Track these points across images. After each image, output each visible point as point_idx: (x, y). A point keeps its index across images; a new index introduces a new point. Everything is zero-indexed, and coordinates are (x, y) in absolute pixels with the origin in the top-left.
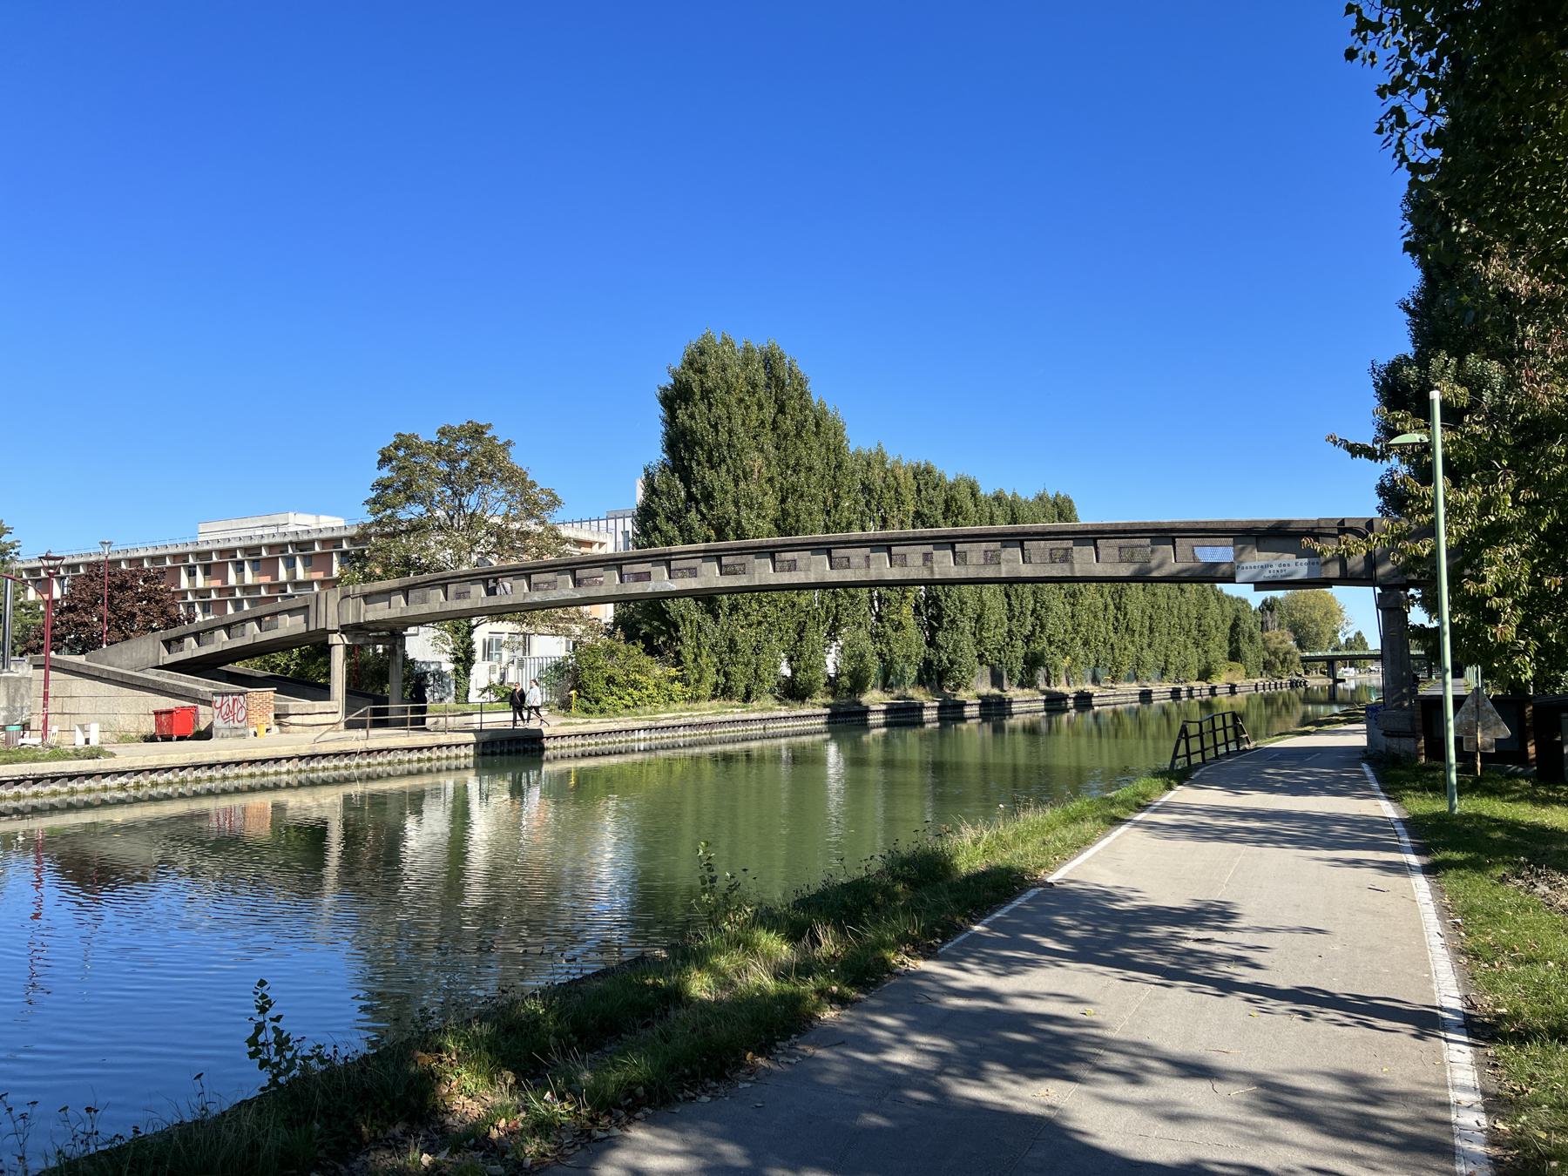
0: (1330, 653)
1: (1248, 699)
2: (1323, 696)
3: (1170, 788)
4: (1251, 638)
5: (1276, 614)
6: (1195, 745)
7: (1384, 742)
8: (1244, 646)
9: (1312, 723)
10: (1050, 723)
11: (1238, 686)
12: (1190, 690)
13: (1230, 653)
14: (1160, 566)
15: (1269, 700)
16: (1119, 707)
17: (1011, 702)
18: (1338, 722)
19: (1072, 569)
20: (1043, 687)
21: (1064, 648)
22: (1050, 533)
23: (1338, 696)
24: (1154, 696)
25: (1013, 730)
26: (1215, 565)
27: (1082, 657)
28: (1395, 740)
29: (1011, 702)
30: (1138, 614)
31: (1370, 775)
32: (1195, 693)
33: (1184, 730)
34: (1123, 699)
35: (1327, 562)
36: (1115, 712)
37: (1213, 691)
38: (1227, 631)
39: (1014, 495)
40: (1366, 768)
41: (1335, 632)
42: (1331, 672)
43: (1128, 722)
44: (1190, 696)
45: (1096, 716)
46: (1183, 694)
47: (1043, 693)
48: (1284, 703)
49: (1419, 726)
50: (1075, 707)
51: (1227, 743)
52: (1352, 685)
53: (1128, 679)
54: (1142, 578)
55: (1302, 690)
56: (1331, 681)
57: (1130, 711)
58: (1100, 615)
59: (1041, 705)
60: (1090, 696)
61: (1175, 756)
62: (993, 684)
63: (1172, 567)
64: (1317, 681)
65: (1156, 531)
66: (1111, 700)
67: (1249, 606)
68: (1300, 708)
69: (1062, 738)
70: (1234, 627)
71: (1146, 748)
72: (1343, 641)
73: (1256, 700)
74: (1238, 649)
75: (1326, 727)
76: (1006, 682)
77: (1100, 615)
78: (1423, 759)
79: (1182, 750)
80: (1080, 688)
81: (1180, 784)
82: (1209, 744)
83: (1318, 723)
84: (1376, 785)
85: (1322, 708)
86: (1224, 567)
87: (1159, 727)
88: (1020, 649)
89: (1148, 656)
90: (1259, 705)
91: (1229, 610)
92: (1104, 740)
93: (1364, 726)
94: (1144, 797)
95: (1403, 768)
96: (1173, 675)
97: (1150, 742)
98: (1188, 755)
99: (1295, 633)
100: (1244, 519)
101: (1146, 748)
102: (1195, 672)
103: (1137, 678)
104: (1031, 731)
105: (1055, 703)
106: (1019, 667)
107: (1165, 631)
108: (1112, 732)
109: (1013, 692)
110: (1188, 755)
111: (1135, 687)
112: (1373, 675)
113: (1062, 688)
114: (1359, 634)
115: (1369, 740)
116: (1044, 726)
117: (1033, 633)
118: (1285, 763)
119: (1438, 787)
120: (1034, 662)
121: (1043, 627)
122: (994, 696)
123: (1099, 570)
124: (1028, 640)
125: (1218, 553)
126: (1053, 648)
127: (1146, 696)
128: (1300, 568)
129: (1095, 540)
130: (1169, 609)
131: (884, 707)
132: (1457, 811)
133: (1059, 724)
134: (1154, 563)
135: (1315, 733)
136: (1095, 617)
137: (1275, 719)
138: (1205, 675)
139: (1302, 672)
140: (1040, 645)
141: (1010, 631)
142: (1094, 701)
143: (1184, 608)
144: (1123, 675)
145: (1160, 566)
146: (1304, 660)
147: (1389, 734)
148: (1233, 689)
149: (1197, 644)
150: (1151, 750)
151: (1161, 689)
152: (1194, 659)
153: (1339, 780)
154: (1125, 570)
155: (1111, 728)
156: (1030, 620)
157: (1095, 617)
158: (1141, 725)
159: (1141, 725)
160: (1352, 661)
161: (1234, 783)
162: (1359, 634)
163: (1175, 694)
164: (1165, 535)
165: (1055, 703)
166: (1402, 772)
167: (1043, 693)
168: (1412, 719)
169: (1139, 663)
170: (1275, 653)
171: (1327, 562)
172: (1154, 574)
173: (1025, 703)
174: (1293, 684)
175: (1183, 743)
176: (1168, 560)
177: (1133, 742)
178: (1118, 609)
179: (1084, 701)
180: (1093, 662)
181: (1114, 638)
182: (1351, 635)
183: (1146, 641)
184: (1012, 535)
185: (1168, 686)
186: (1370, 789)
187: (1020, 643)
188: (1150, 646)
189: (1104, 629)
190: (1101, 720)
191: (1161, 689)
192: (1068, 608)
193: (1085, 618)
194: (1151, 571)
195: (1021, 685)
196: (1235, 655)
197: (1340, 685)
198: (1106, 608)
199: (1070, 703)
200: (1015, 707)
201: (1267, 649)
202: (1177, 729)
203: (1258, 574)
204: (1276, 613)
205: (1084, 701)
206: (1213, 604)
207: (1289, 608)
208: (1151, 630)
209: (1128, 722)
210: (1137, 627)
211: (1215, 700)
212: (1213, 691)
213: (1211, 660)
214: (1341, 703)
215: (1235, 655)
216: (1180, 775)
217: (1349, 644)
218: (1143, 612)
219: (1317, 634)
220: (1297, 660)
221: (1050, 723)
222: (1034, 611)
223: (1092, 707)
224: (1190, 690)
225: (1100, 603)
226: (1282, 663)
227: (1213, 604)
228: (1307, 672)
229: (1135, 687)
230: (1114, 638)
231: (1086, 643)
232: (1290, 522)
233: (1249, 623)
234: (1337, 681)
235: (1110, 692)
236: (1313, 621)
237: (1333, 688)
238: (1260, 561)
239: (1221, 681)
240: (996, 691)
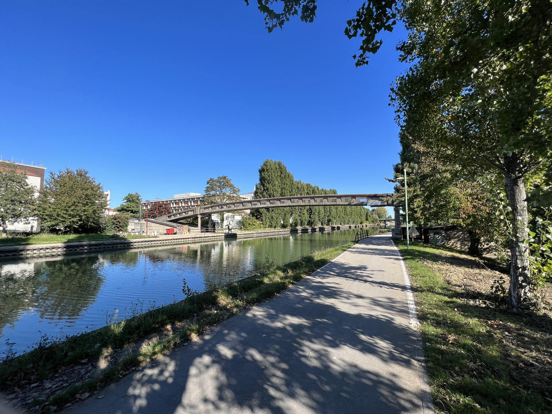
6: (359, 236)
8: (369, 218)
9: (381, 232)
15: (373, 228)
54: (350, 205)
63: (355, 203)
64: (382, 224)
68: (379, 230)
89: (350, 219)
104: (329, 234)
105: (333, 229)
109: (325, 226)
111: (348, 226)
113: (334, 226)
119: (405, 244)
120: (329, 221)
123: (342, 203)
124: (328, 217)
125: (364, 200)
127: (350, 227)
128: (379, 203)
138: (361, 223)
140: (330, 218)
151: (353, 226)
152: (359, 220)
154: (346, 203)
159: (349, 233)
160: (389, 221)
161: (367, 243)
163: (356, 227)
164: (354, 197)
165: (333, 229)
169: (349, 221)
176: (354, 201)
185: (354, 225)
189: (342, 214)
191: (353, 226)
193: (339, 212)
196: (367, 220)
209: (347, 232)
215: (367, 220)
216: (357, 242)
217: (388, 218)
229: (348, 226)
233: (369, 214)
238: (371, 202)
239: (364, 225)
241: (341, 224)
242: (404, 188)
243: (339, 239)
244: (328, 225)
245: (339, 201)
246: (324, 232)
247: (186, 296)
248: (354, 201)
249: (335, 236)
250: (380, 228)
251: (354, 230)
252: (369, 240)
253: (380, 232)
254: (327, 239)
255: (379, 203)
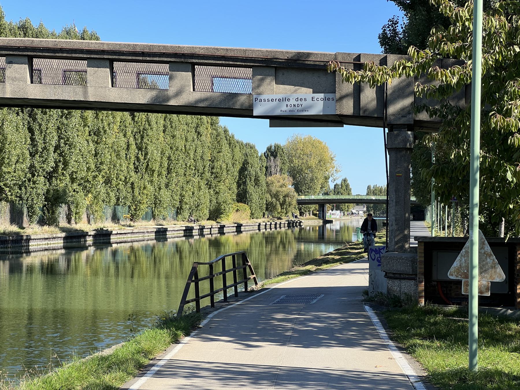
0: (321, 197)
1: (252, 238)
2: (314, 235)
3: (176, 341)
4: (257, 181)
5: (279, 162)
6: (205, 286)
7: (385, 284)
8: (251, 188)
9: (306, 263)
10: (69, 261)
11: (244, 226)
12: (202, 229)
13: (238, 195)
14: (178, 94)
15: (269, 239)
16: (136, 245)
17: (28, 239)
18: (334, 261)
19: (85, 93)
20: (63, 223)
21: (86, 186)
22: (62, 50)
23: (327, 234)
24: (169, 234)
25: (31, 269)
26: (233, 96)
27: (103, 196)
28: (397, 282)
29: (28, 239)
30: (157, 155)
31: (375, 320)
32: (206, 231)
33: (194, 273)
34: (140, 237)
35: (342, 98)
36: (132, 249)
37: (221, 230)
38: (236, 174)
39: (41, 25)
40: (369, 312)
41: (326, 178)
42: (321, 214)
43: (144, 260)
44: (201, 234)
45: (115, 253)
46: (195, 232)
47: (63, 230)
48: (282, 242)
49: (421, 268)
50: (95, 244)
51: (235, 285)
52: (336, 226)
53: (146, 218)
54: (159, 107)
55: (297, 229)
56: (321, 223)
57: (146, 248)
58: (123, 153)
59: (60, 243)
60: (108, 234)
61: (184, 301)
62: (13, 221)
63: (189, 97)
64: (310, 222)
65: (175, 55)
66: (129, 237)
67: (256, 151)
68: (294, 247)
69: (80, 278)
70: (243, 170)
71: (159, 285)
72: (332, 187)
73: (259, 238)
74: (245, 192)
75: (324, 267)
76: (25, 219)
77: (123, 153)
78: (422, 302)
79: (191, 295)
80: (100, 225)
81: (187, 335)
82: (218, 284)
83: (318, 262)
84: (382, 332)
85: (312, 247)
86: (242, 99)
87: (172, 264)
88: (42, 185)
89: (165, 195)
90: (261, 243)
91: (239, 156)
92: (121, 280)
93: (367, 265)
94: (146, 353)
95: (405, 312)
96: (186, 214)
97: (163, 281)
98: (197, 300)
99: (294, 178)
100: (264, 49)
101: (159, 285)
102: (207, 212)
103: (154, 217)
104: (50, 270)
105: (74, 241)
106: (39, 204)
107: (181, 171)
108: (129, 270)
109: (32, 230)
110: (197, 300)
111: (151, 226)
112: (354, 218)
113: (82, 225)
114: (345, 180)
115: (371, 281)
116: (62, 264)
117: (55, 169)
118: (293, 306)
119: (456, 337)
120: (54, 199)
121: (66, 164)
122: (11, 234)
123: (114, 96)
124: (50, 176)
125: (237, 83)
126: (75, 186)
127: (161, 234)
128: (315, 103)
129: (112, 61)
130: (187, 152)
131: (184, 228)
132: (477, 369)
133: (77, 261)
134: (172, 91)
135: (316, 272)
136: (118, 156)
137: (273, 257)
138: (215, 214)
139: (298, 213)
140: (62, 183)
141: (32, 167)
142: (113, 239)
143: (200, 150)
144: (141, 213)
145: (178, 94)
146: (300, 203)
147: (391, 276)
148: (239, 228)
149: (209, 186)
150: (164, 289)
151: (175, 227)
152: (206, 198)
153: (347, 326)
154: (142, 97)
155: (128, 265)
156: (52, 157)
157: (118, 156)
158: (156, 261)
159: (156, 261)
160: (338, 204)
161: (246, 332)
162: (345, 180)
163: (188, 232)
164: (184, 61)
165: (74, 241)
166: (406, 317)
167: (63, 230)
168: (414, 261)
169: (157, 202)
170: (276, 196)
171: (342, 98)
172: (172, 103)
173: (44, 241)
174: (291, 225)
175: (193, 285)
176: (185, 88)
177: (147, 281)
178: (140, 149)
179: (103, 238)
180: (113, 200)
181: (134, 177)
182: (339, 182)
183: (164, 181)
184: (18, 49)
185: (182, 225)
186: (377, 336)
187: (42, 179)
188: (167, 186)
189: (125, 167)
190: (119, 258)
191: (175, 227)
192: (92, 146)
193: (107, 156)
194: (168, 99)
195: (42, 222)
196: (242, 197)
197: (328, 226)
198: (128, 148)
199: (90, 240)
200: (33, 245)
201: (269, 191)
202: (188, 269)
203: (274, 109)
204: (278, 158)
205: (103, 238)
206: (226, 148)
207: (290, 156)
208: (169, 171)
209: (144, 260)
210: (156, 167)
211: (223, 238)
212: (221, 230)
213: (221, 200)
214: (328, 242)
215: (242, 197)
216: (185, 323)
217: (337, 190)
218: (163, 153)
219: (312, 180)
220: (294, 202)
221: (69, 261)
222: (57, 147)
223: (110, 244)
224: (202, 229)
225: (123, 142)
226: (282, 205)
227: (226, 148)
228: (301, 214)
229: (151, 226)
230: (134, 177)
231: (108, 181)
232: (309, 55)
233: (256, 168)
234: (326, 222)
235: (128, 230)
236: (309, 167)
237: (322, 229)
238: (278, 95)
239: (228, 221)
240: (14, 228)
241: (115, 218)
242: (464, 13)
243: (102, 306)
244: (47, 220)
245: (98, 85)
246: (27, 261)
247: (377, 135)
248: (185, 88)
249: (87, 289)
250: (300, 239)
251: (178, 250)
252: (253, 309)
253: (298, 258)
254: (38, 305)
255: (315, 103)
